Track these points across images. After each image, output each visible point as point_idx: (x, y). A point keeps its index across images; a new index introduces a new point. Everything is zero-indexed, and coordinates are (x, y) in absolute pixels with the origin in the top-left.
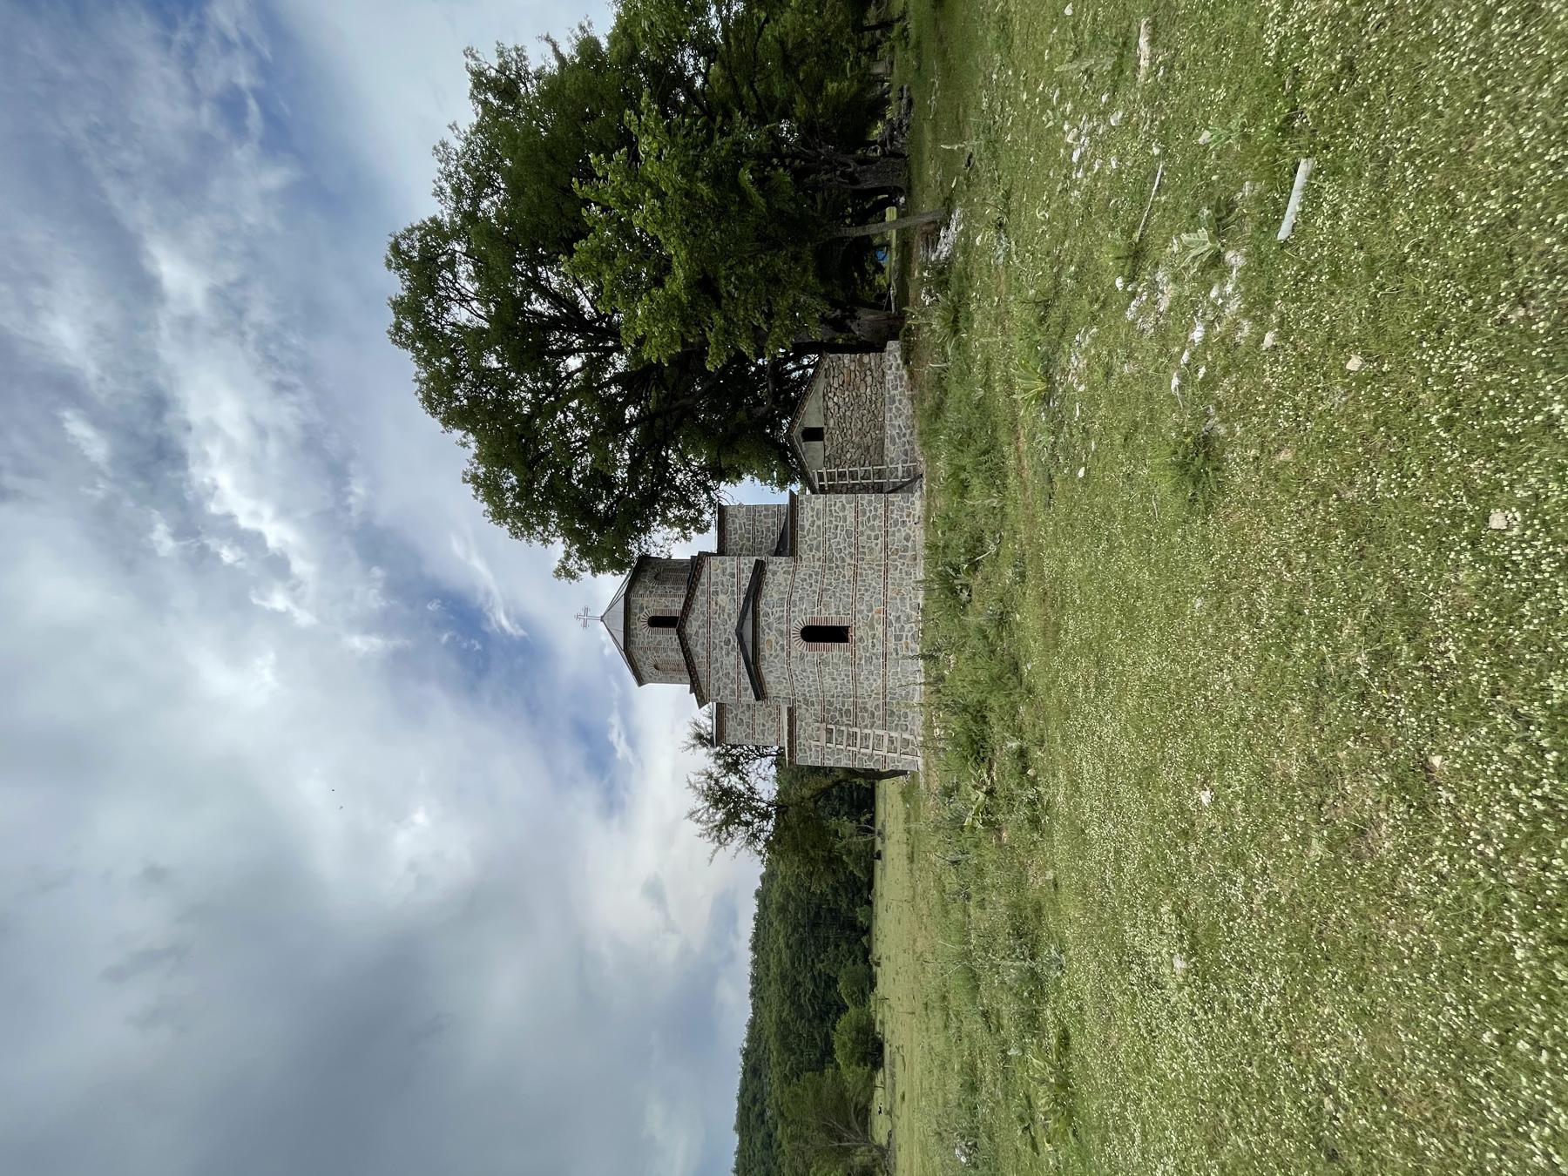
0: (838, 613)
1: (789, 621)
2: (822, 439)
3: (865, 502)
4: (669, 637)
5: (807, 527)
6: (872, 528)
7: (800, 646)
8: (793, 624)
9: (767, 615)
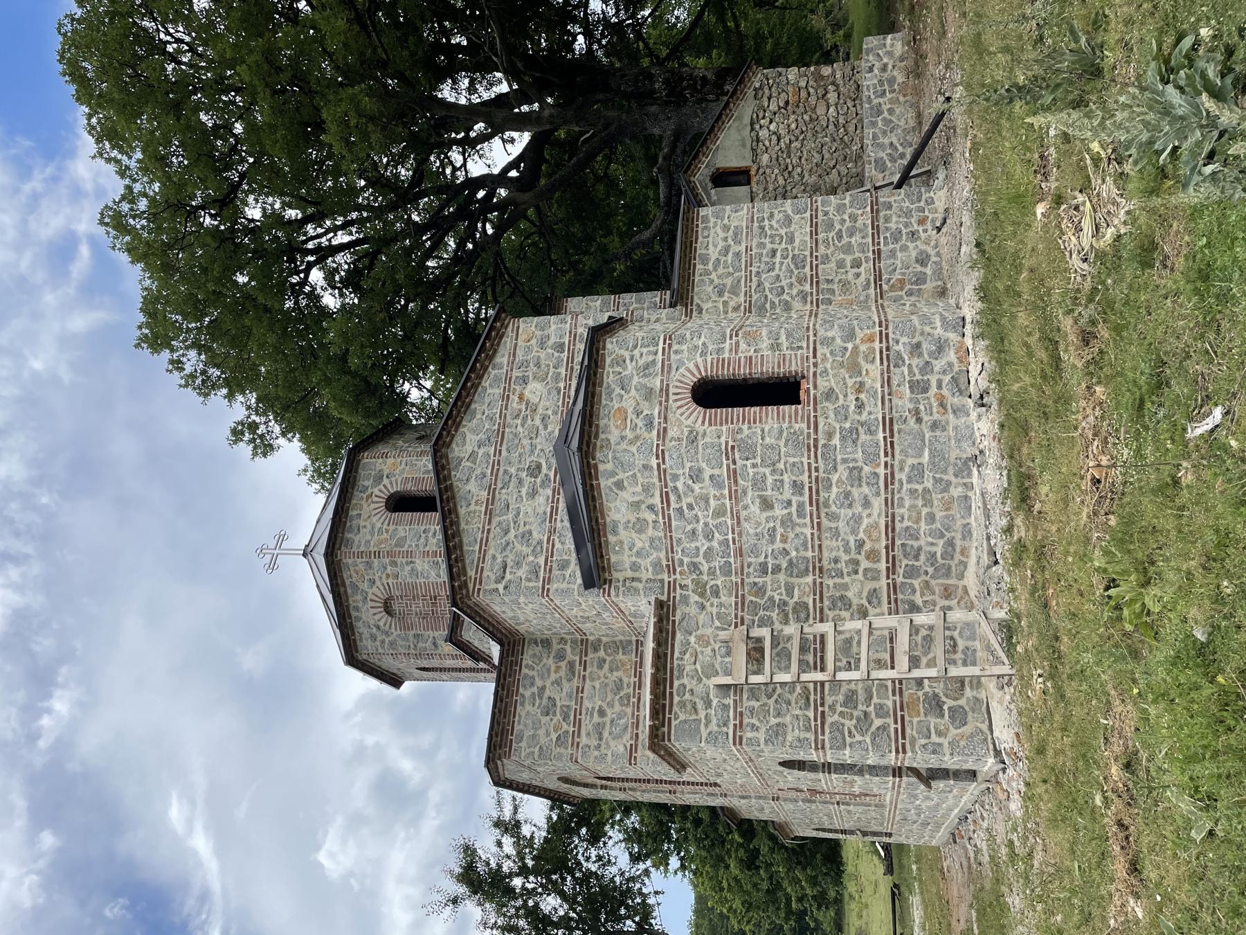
0: (775, 346)
1: (666, 368)
2: (749, 183)
3: (831, 209)
4: (428, 528)
5: (713, 257)
6: (848, 249)
7: (688, 417)
8: (675, 376)
9: (621, 362)
